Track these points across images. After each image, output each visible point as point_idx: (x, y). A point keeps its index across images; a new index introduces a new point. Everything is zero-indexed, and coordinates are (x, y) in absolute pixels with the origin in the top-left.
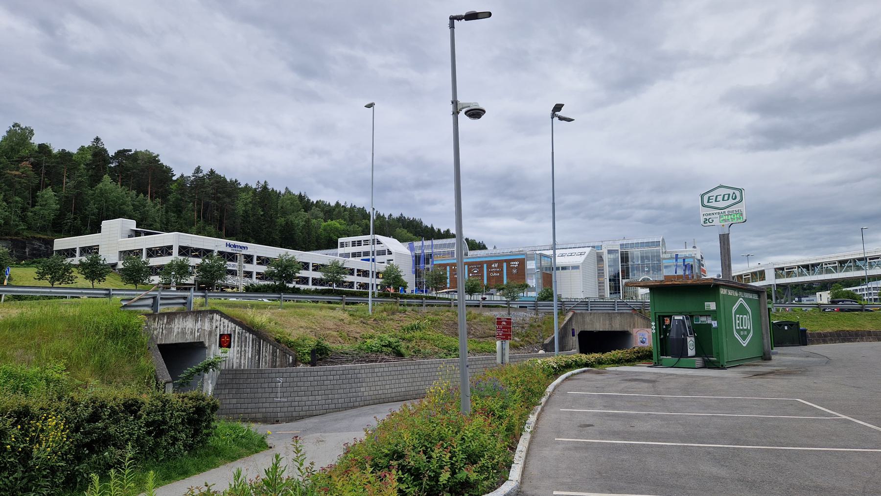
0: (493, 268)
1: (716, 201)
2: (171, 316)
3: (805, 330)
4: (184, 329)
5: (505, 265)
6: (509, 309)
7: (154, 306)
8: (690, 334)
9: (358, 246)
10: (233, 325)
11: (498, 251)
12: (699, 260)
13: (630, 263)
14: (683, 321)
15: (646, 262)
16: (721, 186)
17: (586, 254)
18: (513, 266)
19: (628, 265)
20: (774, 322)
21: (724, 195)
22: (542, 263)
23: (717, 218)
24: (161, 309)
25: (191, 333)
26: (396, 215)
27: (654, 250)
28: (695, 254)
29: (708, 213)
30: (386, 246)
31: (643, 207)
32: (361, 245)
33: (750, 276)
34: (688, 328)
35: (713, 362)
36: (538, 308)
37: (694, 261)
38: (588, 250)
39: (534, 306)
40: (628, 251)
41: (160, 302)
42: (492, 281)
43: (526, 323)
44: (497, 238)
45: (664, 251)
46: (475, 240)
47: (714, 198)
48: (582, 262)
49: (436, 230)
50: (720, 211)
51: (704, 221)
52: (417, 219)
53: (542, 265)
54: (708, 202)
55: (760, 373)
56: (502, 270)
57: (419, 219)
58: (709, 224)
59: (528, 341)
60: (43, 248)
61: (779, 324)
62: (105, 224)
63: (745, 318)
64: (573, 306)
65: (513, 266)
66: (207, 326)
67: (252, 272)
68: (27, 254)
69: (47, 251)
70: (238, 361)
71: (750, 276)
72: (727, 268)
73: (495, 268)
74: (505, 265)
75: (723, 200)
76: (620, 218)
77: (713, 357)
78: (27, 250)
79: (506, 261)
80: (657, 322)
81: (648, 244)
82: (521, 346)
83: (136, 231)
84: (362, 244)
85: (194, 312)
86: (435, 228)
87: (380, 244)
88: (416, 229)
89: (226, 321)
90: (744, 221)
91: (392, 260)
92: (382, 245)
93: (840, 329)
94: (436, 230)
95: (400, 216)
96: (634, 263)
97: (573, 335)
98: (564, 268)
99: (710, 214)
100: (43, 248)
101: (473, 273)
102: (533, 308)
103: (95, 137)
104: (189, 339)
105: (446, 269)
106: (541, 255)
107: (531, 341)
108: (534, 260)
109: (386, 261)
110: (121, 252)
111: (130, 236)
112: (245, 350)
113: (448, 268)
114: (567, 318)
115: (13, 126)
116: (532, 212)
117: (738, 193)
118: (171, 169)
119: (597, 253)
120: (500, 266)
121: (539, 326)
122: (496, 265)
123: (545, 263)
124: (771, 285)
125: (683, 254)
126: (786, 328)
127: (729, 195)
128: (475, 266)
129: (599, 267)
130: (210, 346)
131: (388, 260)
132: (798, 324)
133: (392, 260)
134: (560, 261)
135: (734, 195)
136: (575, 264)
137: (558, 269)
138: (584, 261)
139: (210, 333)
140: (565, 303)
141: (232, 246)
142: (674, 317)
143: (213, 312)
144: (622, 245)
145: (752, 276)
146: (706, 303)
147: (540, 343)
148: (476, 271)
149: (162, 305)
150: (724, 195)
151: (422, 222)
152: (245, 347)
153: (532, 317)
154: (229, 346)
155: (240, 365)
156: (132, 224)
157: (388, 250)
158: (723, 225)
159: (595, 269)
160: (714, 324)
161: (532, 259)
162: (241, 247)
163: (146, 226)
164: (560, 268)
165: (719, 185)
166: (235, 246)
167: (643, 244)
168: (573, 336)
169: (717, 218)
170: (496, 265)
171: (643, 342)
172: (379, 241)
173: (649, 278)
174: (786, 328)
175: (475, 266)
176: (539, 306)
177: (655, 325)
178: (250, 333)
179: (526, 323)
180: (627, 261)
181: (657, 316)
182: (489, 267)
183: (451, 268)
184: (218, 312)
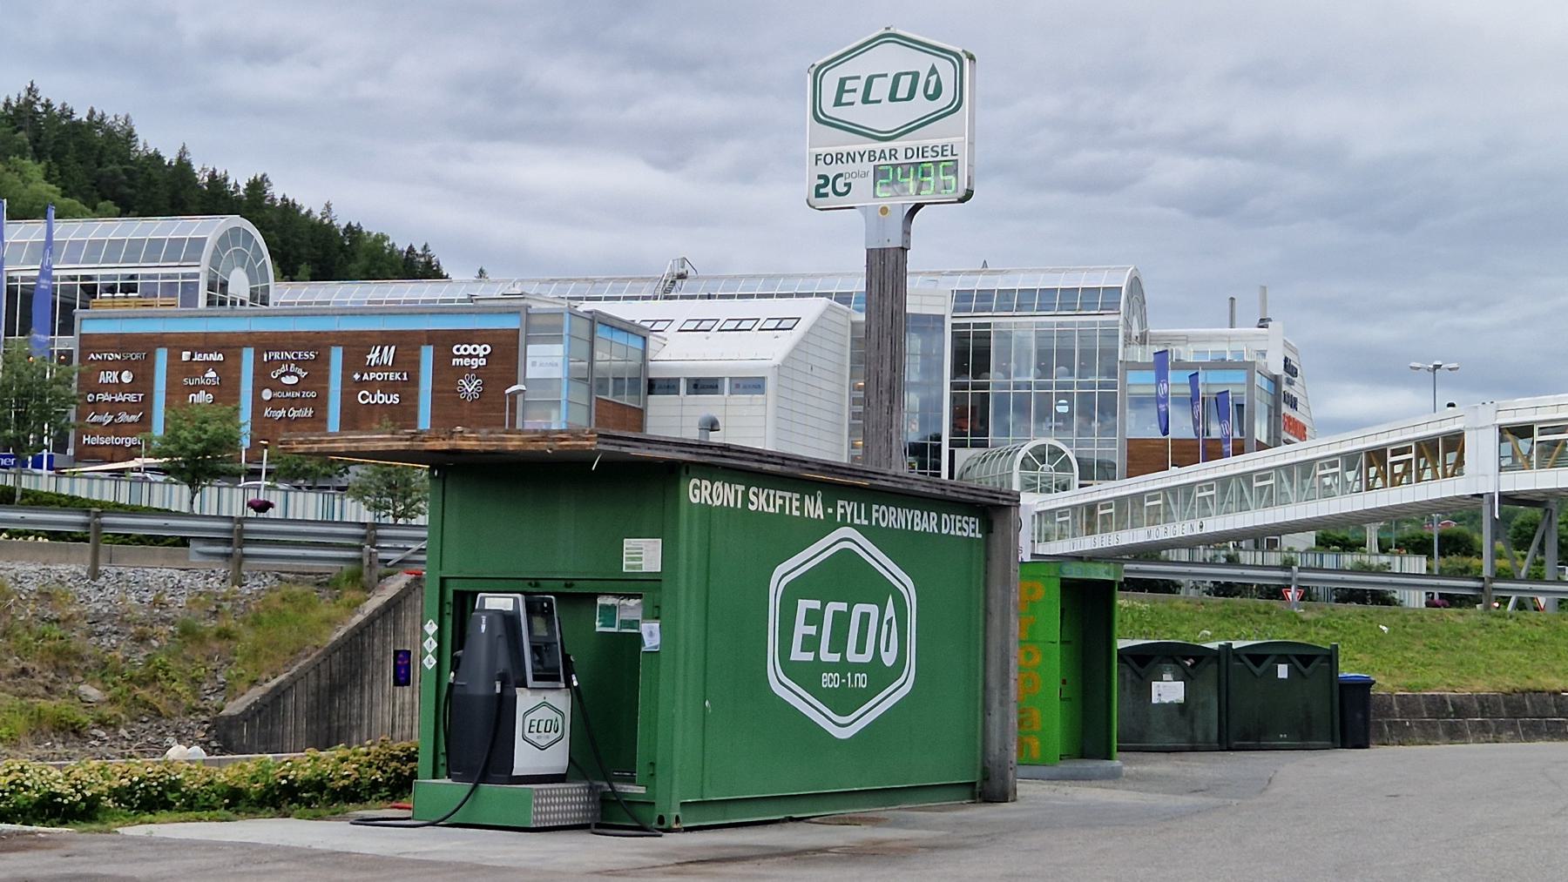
0: (370, 369)
1: (866, 100)
3: (1366, 685)
5: (427, 354)
8: (536, 678)
11: (490, 291)
12: (1275, 380)
13: (994, 376)
14: (510, 620)
15: (1058, 375)
16: (889, 37)
18: (466, 362)
19: (987, 386)
21: (897, 78)
22: (598, 355)
23: (866, 174)
27: (1094, 324)
28: (1263, 354)
29: (833, 150)
31: (1189, 143)
34: (535, 649)
35: (630, 804)
36: (248, 550)
37: (1251, 380)
39: (228, 542)
40: (988, 325)
43: (165, 621)
44: (501, 230)
45: (1136, 331)
46: (385, 238)
47: (860, 86)
48: (777, 361)
49: (203, 178)
50: (878, 146)
51: (818, 187)
52: (109, 120)
53: (597, 364)
54: (838, 103)
55: (742, 852)
56: (414, 380)
57: (122, 116)
58: (833, 200)
59: (146, 704)
61: (1258, 652)
63: (865, 617)
64: (415, 546)
65: (466, 362)
71: (1412, 456)
72: (885, 396)
73: (383, 368)
74: (427, 354)
75: (893, 98)
76: (1092, 184)
77: (631, 781)
79: (432, 337)
80: (449, 621)
81: (1068, 299)
82: (102, 723)
86: (197, 168)
88: (100, 165)
90: (961, 194)
93: (1530, 684)
94: (203, 178)
95: (24, 94)
96: (1008, 376)
97: (402, 678)
101: (277, 386)
102: (221, 549)
105: (323, 361)
106: (595, 320)
107: (163, 704)
108: (558, 339)
113: (162, 356)
114: (375, 602)
116: (723, 132)
117: (946, 70)
120: (407, 361)
121: (224, 635)
122: (388, 355)
123: (611, 356)
124: (1481, 496)
125: (1211, 347)
126: (1283, 671)
127: (916, 75)
128: (291, 356)
132: (1331, 657)
135: (933, 79)
138: (790, 357)
140: (380, 532)
142: (483, 599)
144: (962, 298)
145: (1420, 455)
146: (628, 543)
147: (204, 711)
148: (293, 380)
150: (897, 78)
151: (130, 134)
153: (208, 593)
158: (884, 210)
159: (842, 396)
160: (651, 634)
161: (551, 334)
164: (683, 386)
165: (882, 31)
167: (1047, 299)
168: (397, 683)
169: (866, 174)
170: (388, 355)
173: (1062, 447)
174: (1283, 671)
175: (291, 356)
176: (257, 542)
177: (440, 636)
179: (165, 621)
180: (982, 366)
181: (450, 596)
183: (174, 358)
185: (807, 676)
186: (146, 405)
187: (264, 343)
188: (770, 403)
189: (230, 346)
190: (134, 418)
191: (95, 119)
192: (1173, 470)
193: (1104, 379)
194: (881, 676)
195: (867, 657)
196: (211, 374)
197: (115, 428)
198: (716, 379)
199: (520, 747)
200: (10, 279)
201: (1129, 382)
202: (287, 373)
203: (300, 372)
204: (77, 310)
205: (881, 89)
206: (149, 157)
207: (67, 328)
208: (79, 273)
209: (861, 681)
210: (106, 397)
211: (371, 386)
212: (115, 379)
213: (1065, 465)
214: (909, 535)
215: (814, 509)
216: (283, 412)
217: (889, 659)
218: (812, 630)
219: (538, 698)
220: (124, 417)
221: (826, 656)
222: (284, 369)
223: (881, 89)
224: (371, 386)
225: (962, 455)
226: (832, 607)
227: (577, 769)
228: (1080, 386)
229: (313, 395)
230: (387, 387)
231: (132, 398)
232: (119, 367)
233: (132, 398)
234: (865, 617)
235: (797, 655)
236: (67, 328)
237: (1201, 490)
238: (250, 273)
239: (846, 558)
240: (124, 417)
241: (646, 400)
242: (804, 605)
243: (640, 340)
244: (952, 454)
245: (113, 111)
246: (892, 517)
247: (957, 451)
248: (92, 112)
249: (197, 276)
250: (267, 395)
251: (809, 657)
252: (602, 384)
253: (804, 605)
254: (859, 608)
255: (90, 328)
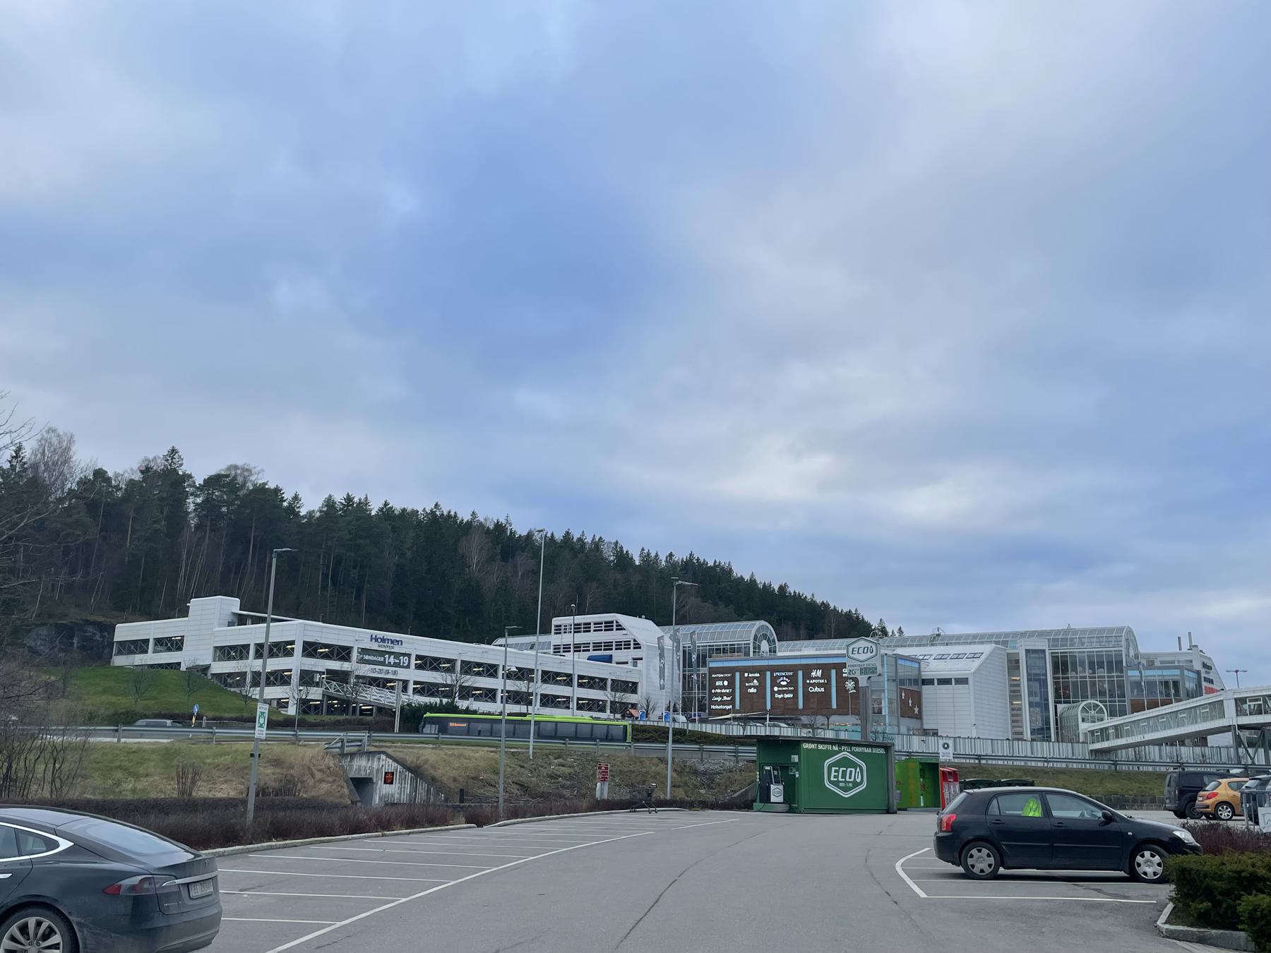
0: (813, 678)
2: (352, 755)
4: (360, 766)
5: (833, 672)
6: (702, 753)
7: (342, 747)
9: (584, 632)
10: (396, 765)
17: (983, 657)
20: (1002, 780)
24: (347, 750)
25: (365, 770)
26: (681, 556)
30: (632, 634)
32: (590, 631)
33: (1261, 702)
36: (739, 754)
38: (986, 649)
39: (734, 752)
41: (347, 744)
42: (812, 700)
47: (857, 650)
48: (972, 671)
60: (98, 637)
62: (195, 604)
63: (851, 772)
66: (375, 765)
67: (408, 681)
68: (75, 645)
69: (103, 641)
70: (398, 796)
73: (817, 678)
74: (833, 672)
78: (75, 641)
83: (240, 615)
84: (592, 629)
85: (366, 753)
86: (758, 582)
87: (621, 629)
88: (719, 584)
89: (390, 761)
91: (641, 659)
92: (624, 632)
94: (761, 586)
98: (945, 682)
99: (853, 666)
100: (98, 637)
102: (733, 754)
103: (170, 448)
104: (363, 775)
105: (796, 675)
109: (630, 661)
110: (216, 648)
111: (230, 624)
112: (405, 787)
115: (48, 432)
118: (281, 490)
119: (1008, 654)
122: (819, 673)
123: (906, 670)
129: (1013, 680)
130: (377, 782)
131: (634, 659)
133: (641, 659)
134: (934, 669)
136: (960, 674)
137: (930, 682)
138: (978, 669)
139: (378, 770)
141: (379, 640)
143: (380, 753)
148: (784, 683)
149: (347, 746)
152: (405, 783)
154: (392, 783)
155: (400, 801)
156: (233, 605)
157: (635, 640)
162: (392, 642)
163: (253, 610)
164: (936, 682)
166: (383, 640)
170: (819, 673)
171: (295, 759)
172: (620, 626)
178: (409, 772)
182: (807, 676)
183: (742, 675)
184: (384, 753)
185: (836, 784)
186: (732, 694)
187: (773, 669)
188: (971, 689)
189: (762, 670)
190: (729, 698)
191: (717, 564)
192: (1119, 718)
193: (1118, 674)
194: (856, 784)
195: (852, 780)
196: (755, 681)
197: (722, 703)
198: (1009, 661)
199: (772, 796)
200: (684, 647)
201: (1129, 675)
202: (783, 681)
203: (787, 680)
204: (708, 658)
205: (861, 651)
206: (739, 579)
207: (704, 664)
208: (708, 644)
209: (851, 785)
210: (719, 691)
211: (814, 685)
212: (722, 684)
213: (1101, 711)
214: (863, 753)
215: (836, 748)
216: (781, 696)
217: (859, 780)
218: (836, 774)
219: (775, 787)
220: (725, 698)
221: (840, 779)
222: (781, 679)
223: (861, 651)
224: (814, 685)
225: (1060, 707)
226: (841, 769)
227: (785, 801)
228: (1108, 677)
229: (792, 688)
230: (819, 685)
231: (728, 691)
232: (723, 679)
233: (728, 691)
234: (851, 772)
235: (832, 779)
236: (704, 664)
237: (1142, 723)
238: (769, 641)
239: (845, 758)
240: (725, 698)
241: (921, 688)
242: (833, 769)
243: (918, 664)
244: (1056, 706)
245: (723, 561)
246: (858, 749)
247: (1058, 705)
248: (715, 561)
249: (749, 644)
250: (776, 689)
251: (836, 779)
252: (902, 682)
253: (833, 769)
254: (849, 770)
255: (712, 665)
